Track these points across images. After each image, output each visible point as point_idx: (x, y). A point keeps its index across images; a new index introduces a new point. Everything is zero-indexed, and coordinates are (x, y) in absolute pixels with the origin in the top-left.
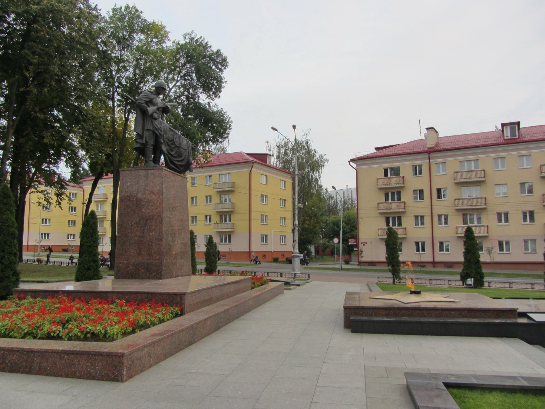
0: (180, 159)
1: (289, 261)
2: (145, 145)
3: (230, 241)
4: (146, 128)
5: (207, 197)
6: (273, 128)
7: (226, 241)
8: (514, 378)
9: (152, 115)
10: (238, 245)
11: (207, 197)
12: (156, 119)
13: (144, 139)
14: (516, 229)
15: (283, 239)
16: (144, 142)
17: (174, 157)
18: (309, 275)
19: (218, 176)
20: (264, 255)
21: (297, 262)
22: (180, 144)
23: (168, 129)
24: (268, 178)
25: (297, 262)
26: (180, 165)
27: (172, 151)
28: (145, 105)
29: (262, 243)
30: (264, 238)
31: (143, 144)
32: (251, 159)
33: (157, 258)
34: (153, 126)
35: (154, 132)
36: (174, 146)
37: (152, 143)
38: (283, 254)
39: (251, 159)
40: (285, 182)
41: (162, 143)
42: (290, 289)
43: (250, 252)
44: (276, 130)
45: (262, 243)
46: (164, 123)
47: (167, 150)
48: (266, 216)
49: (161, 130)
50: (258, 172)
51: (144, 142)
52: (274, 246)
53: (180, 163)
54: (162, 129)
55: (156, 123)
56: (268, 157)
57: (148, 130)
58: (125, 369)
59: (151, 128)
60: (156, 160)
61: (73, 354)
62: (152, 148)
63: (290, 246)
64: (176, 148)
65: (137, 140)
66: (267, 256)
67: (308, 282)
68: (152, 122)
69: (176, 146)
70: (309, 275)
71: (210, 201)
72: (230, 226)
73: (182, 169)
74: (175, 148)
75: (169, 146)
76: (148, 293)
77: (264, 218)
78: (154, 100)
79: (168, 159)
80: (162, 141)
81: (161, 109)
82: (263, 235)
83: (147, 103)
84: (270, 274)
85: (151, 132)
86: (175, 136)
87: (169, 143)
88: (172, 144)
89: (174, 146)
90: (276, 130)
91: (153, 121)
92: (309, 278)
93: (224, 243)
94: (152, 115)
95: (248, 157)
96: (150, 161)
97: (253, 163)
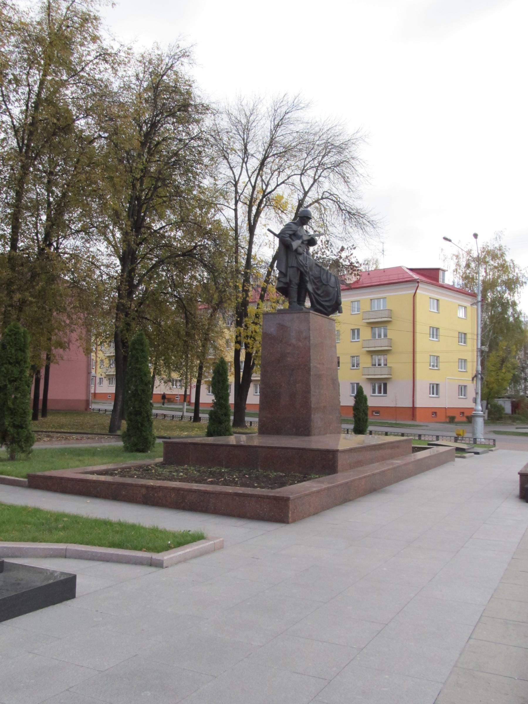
0: (327, 299)
1: (470, 420)
3: (385, 392)
4: (290, 265)
5: (353, 330)
6: (445, 239)
7: (380, 392)
9: (296, 250)
10: (396, 397)
11: (353, 330)
12: (300, 254)
13: (288, 278)
15: (462, 389)
16: (288, 281)
17: (321, 297)
18: (494, 440)
19: (369, 301)
20: (434, 412)
21: (480, 422)
23: (314, 265)
24: (440, 302)
25: (480, 422)
28: (288, 239)
29: (431, 395)
30: (435, 388)
32: (416, 276)
33: (304, 412)
34: (298, 262)
35: (298, 269)
37: (297, 282)
38: (462, 412)
39: (416, 276)
40: (465, 307)
41: (307, 282)
42: (464, 457)
43: (414, 408)
44: (450, 241)
45: (431, 395)
47: (313, 289)
48: (438, 357)
49: (306, 267)
50: (425, 293)
51: (288, 281)
52: (449, 400)
54: (308, 265)
55: (301, 258)
56: (441, 273)
57: (292, 267)
58: (290, 512)
59: (295, 265)
61: (244, 496)
62: (297, 287)
63: (471, 401)
64: (324, 286)
65: (281, 279)
66: (438, 414)
67: (492, 450)
68: (296, 258)
69: (324, 284)
70: (494, 440)
71: (358, 334)
72: (385, 370)
73: (330, 310)
75: (315, 284)
76: (299, 449)
77: (436, 362)
78: (298, 232)
79: (314, 299)
80: (307, 279)
81: (306, 242)
82: (433, 384)
83: (290, 236)
84: (440, 437)
85: (295, 269)
86: (322, 271)
87: (315, 281)
90: (450, 241)
92: (494, 445)
93: (377, 394)
94: (296, 250)
95: (411, 273)
97: (418, 282)
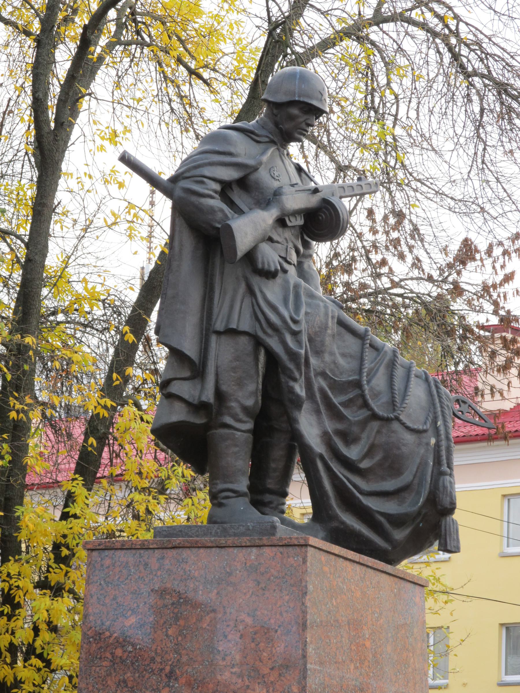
0: (389, 485)
2: (211, 411)
4: (219, 326)
8: (479, 447)
12: (270, 275)
14: (223, 68)
16: (209, 395)
22: (392, 404)
26: (388, 516)
27: (348, 438)
28: (216, 203)
31: (200, 407)
34: (257, 315)
35: (258, 343)
36: (364, 414)
37: (250, 402)
41: (298, 403)
46: (311, 296)
49: (295, 334)
51: (209, 395)
53: (390, 507)
55: (272, 291)
57: (232, 332)
59: (246, 325)
60: (266, 493)
62: (249, 425)
64: (375, 425)
65: (175, 388)
69: (375, 416)
73: (399, 535)
74: (364, 424)
75: (335, 413)
80: (300, 389)
83: (226, 188)
87: (336, 401)
88: (347, 404)
89: (364, 414)
91: (256, 281)
96: (238, 494)
